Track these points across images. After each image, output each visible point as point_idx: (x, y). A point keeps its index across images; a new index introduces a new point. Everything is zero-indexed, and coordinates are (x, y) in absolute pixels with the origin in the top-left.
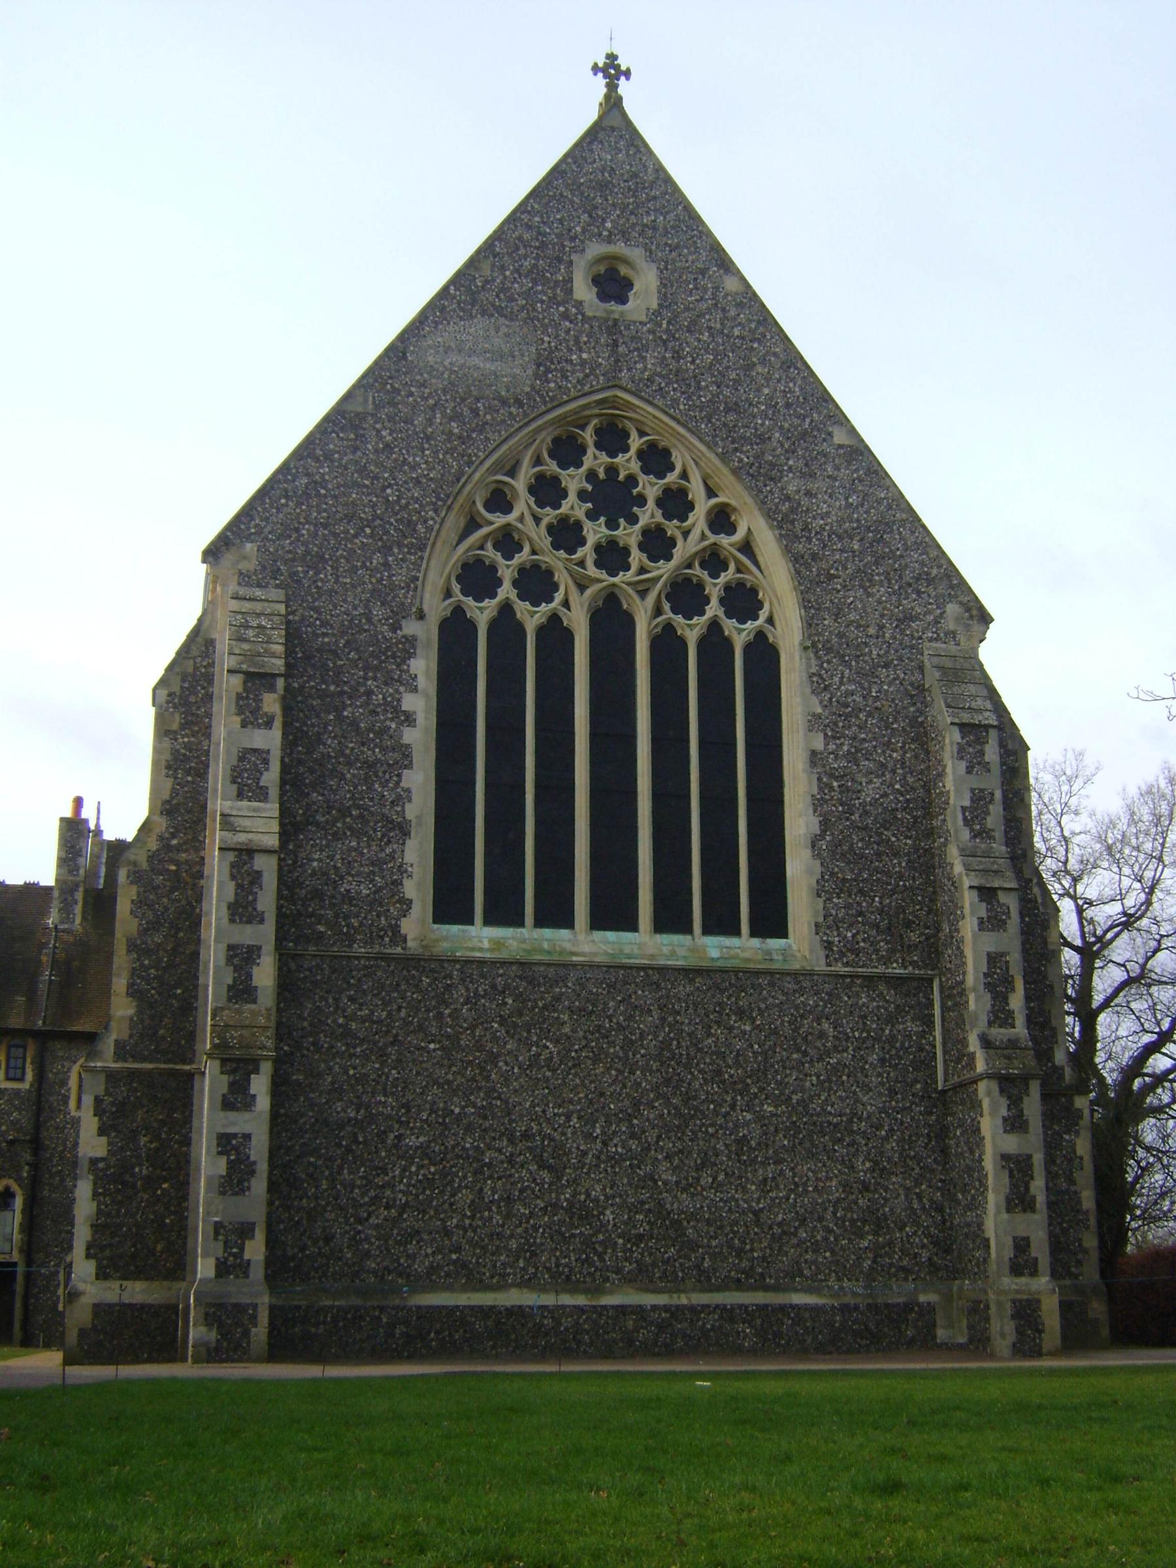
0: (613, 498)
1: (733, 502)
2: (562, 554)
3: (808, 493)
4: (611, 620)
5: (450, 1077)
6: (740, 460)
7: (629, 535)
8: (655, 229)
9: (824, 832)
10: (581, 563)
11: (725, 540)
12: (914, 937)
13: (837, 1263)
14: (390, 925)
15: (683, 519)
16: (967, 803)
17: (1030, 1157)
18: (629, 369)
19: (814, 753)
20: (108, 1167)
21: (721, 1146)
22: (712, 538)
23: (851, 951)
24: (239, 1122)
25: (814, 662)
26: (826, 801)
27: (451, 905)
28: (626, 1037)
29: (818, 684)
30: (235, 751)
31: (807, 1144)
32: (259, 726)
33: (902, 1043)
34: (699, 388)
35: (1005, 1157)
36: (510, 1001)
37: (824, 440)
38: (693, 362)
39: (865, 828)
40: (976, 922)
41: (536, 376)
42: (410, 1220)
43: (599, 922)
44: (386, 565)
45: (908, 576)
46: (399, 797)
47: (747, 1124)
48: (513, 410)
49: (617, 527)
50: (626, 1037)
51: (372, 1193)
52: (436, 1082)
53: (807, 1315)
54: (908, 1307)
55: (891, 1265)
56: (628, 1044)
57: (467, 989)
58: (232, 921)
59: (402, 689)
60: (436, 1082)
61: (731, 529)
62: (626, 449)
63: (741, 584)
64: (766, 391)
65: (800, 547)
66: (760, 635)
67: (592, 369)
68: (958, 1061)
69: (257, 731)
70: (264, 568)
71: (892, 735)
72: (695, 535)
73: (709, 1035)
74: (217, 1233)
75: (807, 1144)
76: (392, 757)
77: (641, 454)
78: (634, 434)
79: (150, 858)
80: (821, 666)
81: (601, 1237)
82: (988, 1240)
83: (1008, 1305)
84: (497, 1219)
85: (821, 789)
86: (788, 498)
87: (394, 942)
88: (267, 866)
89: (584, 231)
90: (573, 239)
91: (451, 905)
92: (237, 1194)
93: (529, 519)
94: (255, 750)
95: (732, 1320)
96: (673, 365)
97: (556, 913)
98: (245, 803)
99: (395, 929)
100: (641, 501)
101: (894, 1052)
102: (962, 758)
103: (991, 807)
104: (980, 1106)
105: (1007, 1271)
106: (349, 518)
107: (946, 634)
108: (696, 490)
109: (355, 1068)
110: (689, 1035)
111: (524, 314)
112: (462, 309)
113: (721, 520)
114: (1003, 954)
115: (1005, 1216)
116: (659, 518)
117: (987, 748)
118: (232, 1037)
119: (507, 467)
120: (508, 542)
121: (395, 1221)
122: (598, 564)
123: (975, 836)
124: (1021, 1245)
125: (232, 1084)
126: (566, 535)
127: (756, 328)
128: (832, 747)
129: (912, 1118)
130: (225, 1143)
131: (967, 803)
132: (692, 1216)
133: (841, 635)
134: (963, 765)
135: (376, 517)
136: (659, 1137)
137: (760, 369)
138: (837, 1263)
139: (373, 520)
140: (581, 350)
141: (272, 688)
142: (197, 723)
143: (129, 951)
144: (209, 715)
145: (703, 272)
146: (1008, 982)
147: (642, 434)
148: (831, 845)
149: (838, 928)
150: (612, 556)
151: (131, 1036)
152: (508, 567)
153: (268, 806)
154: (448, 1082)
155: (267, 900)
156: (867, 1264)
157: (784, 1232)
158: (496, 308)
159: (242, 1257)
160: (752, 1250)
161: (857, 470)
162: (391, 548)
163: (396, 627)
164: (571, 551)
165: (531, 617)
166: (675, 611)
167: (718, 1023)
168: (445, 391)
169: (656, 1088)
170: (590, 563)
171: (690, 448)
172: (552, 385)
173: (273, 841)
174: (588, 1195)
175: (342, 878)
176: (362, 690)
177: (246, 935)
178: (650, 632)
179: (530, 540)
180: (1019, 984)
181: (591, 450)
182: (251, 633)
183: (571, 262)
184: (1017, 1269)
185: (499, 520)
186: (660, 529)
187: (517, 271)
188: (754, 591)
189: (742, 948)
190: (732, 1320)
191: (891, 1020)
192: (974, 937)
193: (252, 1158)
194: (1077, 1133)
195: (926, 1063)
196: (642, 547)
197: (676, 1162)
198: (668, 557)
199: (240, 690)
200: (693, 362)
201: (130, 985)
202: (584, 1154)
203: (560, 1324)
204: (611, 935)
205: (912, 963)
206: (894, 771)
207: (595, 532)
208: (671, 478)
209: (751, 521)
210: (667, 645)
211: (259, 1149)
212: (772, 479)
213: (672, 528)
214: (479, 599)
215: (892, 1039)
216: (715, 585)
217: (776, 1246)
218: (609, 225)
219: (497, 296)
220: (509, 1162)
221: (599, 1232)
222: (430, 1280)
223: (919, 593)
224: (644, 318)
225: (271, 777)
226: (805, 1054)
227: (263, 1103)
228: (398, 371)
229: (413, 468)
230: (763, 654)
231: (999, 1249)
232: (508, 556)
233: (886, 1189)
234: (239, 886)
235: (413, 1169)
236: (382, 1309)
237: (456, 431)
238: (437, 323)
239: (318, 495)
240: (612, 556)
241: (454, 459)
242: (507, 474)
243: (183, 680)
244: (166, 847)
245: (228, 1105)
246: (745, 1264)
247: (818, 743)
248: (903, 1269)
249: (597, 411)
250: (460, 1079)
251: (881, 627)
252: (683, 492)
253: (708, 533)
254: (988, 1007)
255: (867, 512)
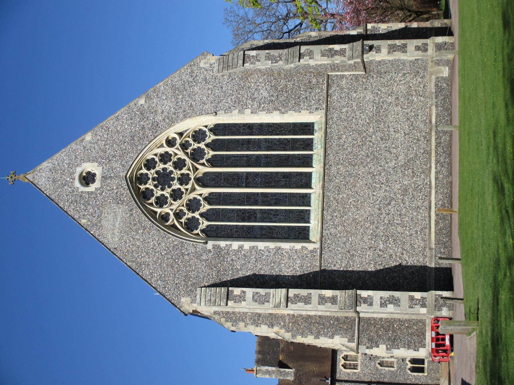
0: (163, 179)
1: (165, 138)
2: (184, 196)
3: (162, 113)
4: (204, 181)
5: (360, 234)
6: (151, 135)
7: (176, 174)
8: (69, 163)
9: (279, 110)
10: (187, 190)
11: (178, 141)
12: (314, 81)
13: (422, 108)
14: (310, 253)
15: (171, 155)
16: (270, 62)
17: (389, 45)
18: (119, 173)
19: (252, 113)
20: (389, 344)
21: (383, 146)
22: (178, 145)
23: (319, 101)
24: (377, 301)
25: (220, 112)
26: (268, 109)
27: (303, 235)
28: (347, 176)
29: (228, 110)
30: (253, 303)
31: (383, 117)
32: (245, 295)
33: (350, 85)
34: (126, 149)
35: (389, 53)
36: (335, 214)
37: (143, 107)
38: (117, 151)
39: (277, 96)
40: (311, 60)
41: (122, 204)
42: (407, 247)
43: (308, 185)
44: (188, 255)
45: (191, 79)
46: (267, 250)
47: (376, 137)
48: (134, 212)
49: (174, 178)
50: (347, 176)
51: (398, 259)
52: (362, 238)
53: (438, 119)
54: (437, 85)
55: (423, 91)
56: (350, 175)
57: (332, 228)
58: (310, 303)
59: (231, 249)
60: (362, 238)
61: (174, 139)
62: (147, 174)
63: (193, 136)
64: (126, 126)
65: (181, 116)
66: (211, 130)
67: (119, 185)
68: (356, 67)
69: (247, 296)
70: (189, 295)
71: (245, 86)
72: (177, 151)
73: (347, 149)
74: (412, 307)
75: (383, 117)
76: (254, 253)
77: (148, 169)
78: (141, 172)
79: (288, 332)
80: (222, 109)
81: (413, 185)
82: (416, 59)
83: (437, 53)
84: (407, 219)
85: (264, 111)
86: (164, 119)
87: (316, 252)
88: (292, 292)
89: (71, 188)
90: (73, 192)
91: (303, 235)
92: (400, 301)
93: (172, 207)
94: (253, 297)
95: (440, 143)
96: (118, 158)
97: (305, 199)
98: (271, 300)
99: (312, 251)
100: (164, 169)
101: (353, 88)
102: (255, 63)
103: (271, 54)
104: (372, 60)
105: (426, 53)
106: (172, 267)
107: (211, 67)
108: (161, 151)
109: (357, 265)
110: (347, 155)
111: (101, 208)
112: (99, 229)
113: (170, 143)
114: (321, 51)
115: (408, 53)
116: (171, 163)
117: (251, 55)
118: (349, 303)
119: (153, 214)
120: (178, 215)
121: (408, 252)
122: (187, 184)
123: (281, 59)
124: (418, 48)
125: (364, 303)
126: (176, 195)
127: (104, 129)
128: (250, 107)
129: (375, 83)
130: (383, 305)
131: (270, 62)
132: (406, 155)
133: (212, 103)
134: (257, 63)
135: (172, 258)
136: (380, 166)
137: (119, 129)
138: (422, 108)
139: (173, 259)
140: (113, 189)
141: (232, 292)
142: (242, 317)
143: (319, 338)
144: (239, 313)
145: (85, 147)
146: (330, 50)
147: (141, 169)
148: (283, 107)
149: (311, 106)
150: (184, 180)
151: (346, 337)
152: (188, 214)
153: (272, 292)
154: (362, 234)
155: (304, 292)
156: (422, 99)
157: (412, 125)
158: (98, 218)
159: (420, 300)
160: (417, 136)
161: (154, 96)
162: (183, 253)
163: (210, 251)
164: (182, 193)
165: (205, 207)
166: (203, 158)
167: (343, 146)
168: (128, 235)
169: (364, 167)
170: (187, 187)
171: (147, 152)
172: (125, 199)
173: (284, 290)
174: (399, 189)
175: (295, 269)
176: (231, 262)
177: (315, 299)
178: (211, 167)
179: (178, 207)
180: (331, 46)
181: (147, 186)
182: (213, 299)
183: (82, 192)
184: (426, 50)
185: (172, 217)
186: (174, 163)
187: (85, 210)
188: (195, 132)
189: (318, 137)
190: (440, 143)
191: (342, 89)
192: (316, 60)
193: (388, 296)
194: (379, 28)
195: (357, 77)
196: (181, 169)
197: (389, 160)
198: (184, 160)
199: (233, 302)
200: (117, 151)
201: (330, 337)
202: (386, 190)
203: (441, 199)
204: (313, 181)
205: (323, 81)
206: (258, 86)
207: (176, 185)
208: (157, 159)
209: (171, 133)
210: (213, 162)
211: (386, 294)
212: (157, 125)
213: (174, 159)
214: (199, 224)
215: (349, 89)
216: (194, 145)
217: (416, 128)
218: (68, 179)
219: (94, 217)
220: (388, 214)
221: (411, 186)
222: (426, 241)
223: (196, 76)
224: (101, 168)
225: (262, 291)
226: (353, 117)
227: (370, 293)
228: (121, 251)
229: (155, 246)
230: (217, 129)
231: (419, 55)
232: (185, 214)
233: (398, 92)
234: (299, 301)
235: (390, 246)
236: (436, 256)
237: (142, 231)
238: (104, 237)
239: (164, 277)
240: (184, 180)
241: (151, 232)
242: (156, 215)
243: (228, 321)
244: (284, 326)
245: (371, 304)
246: (422, 138)
247: (248, 111)
248: (424, 87)
249: (134, 184)
250: (361, 230)
251: (209, 89)
252: (161, 155)
253: (176, 147)
254: (339, 57)
255: (169, 93)
